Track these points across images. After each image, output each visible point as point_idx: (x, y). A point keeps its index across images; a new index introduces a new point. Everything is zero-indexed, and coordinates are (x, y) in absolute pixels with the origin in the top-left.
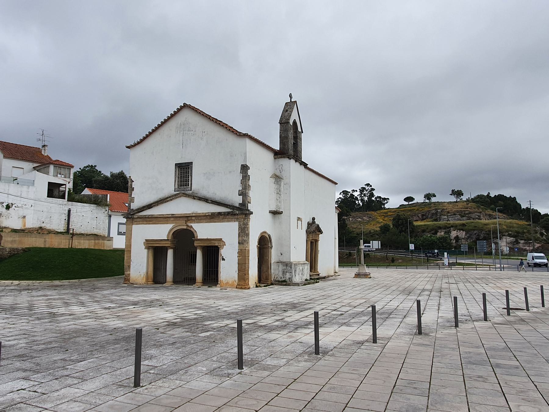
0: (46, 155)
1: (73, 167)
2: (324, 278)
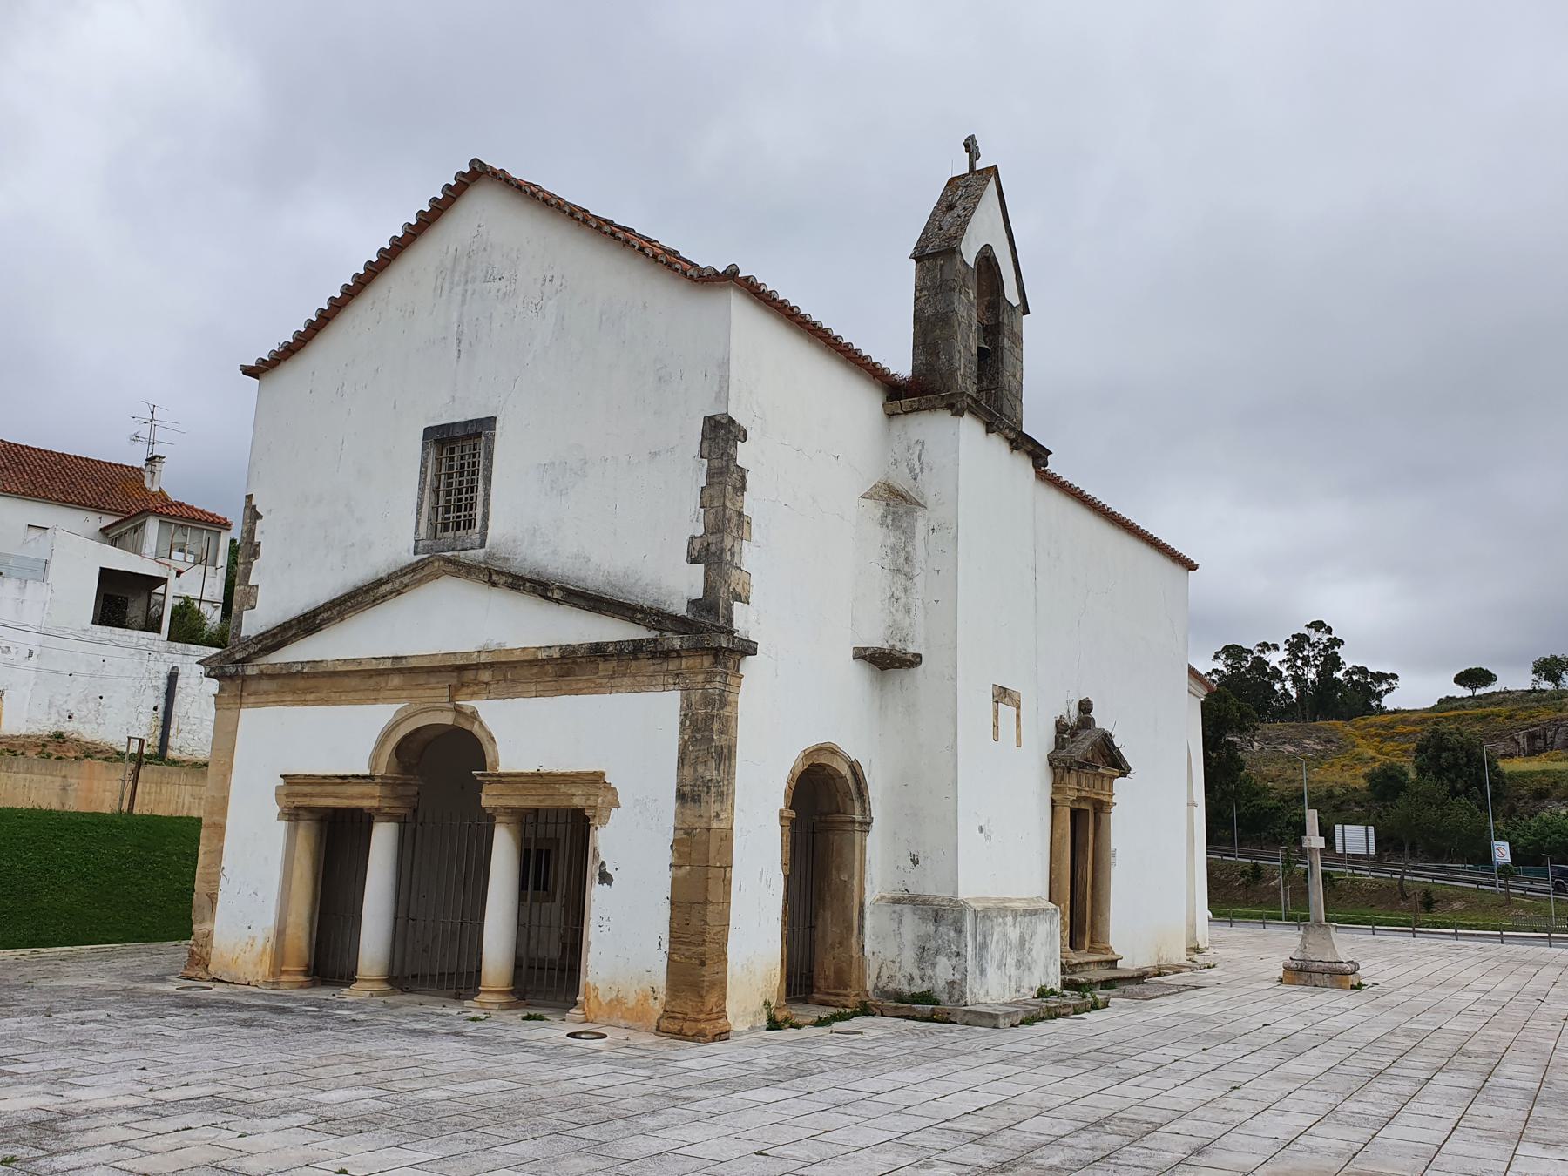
0: (155, 489)
1: (226, 525)
2: (1139, 978)
